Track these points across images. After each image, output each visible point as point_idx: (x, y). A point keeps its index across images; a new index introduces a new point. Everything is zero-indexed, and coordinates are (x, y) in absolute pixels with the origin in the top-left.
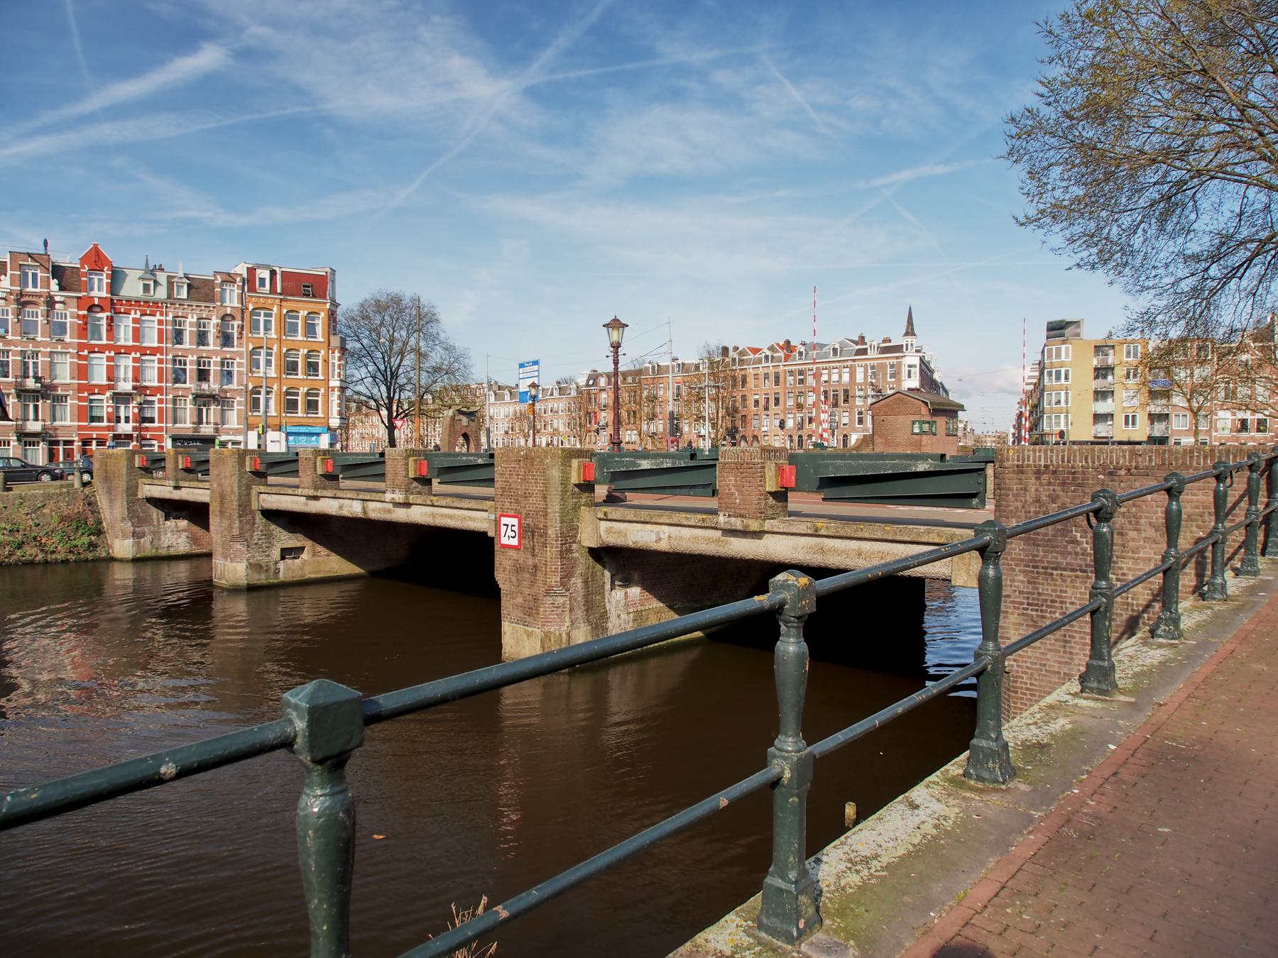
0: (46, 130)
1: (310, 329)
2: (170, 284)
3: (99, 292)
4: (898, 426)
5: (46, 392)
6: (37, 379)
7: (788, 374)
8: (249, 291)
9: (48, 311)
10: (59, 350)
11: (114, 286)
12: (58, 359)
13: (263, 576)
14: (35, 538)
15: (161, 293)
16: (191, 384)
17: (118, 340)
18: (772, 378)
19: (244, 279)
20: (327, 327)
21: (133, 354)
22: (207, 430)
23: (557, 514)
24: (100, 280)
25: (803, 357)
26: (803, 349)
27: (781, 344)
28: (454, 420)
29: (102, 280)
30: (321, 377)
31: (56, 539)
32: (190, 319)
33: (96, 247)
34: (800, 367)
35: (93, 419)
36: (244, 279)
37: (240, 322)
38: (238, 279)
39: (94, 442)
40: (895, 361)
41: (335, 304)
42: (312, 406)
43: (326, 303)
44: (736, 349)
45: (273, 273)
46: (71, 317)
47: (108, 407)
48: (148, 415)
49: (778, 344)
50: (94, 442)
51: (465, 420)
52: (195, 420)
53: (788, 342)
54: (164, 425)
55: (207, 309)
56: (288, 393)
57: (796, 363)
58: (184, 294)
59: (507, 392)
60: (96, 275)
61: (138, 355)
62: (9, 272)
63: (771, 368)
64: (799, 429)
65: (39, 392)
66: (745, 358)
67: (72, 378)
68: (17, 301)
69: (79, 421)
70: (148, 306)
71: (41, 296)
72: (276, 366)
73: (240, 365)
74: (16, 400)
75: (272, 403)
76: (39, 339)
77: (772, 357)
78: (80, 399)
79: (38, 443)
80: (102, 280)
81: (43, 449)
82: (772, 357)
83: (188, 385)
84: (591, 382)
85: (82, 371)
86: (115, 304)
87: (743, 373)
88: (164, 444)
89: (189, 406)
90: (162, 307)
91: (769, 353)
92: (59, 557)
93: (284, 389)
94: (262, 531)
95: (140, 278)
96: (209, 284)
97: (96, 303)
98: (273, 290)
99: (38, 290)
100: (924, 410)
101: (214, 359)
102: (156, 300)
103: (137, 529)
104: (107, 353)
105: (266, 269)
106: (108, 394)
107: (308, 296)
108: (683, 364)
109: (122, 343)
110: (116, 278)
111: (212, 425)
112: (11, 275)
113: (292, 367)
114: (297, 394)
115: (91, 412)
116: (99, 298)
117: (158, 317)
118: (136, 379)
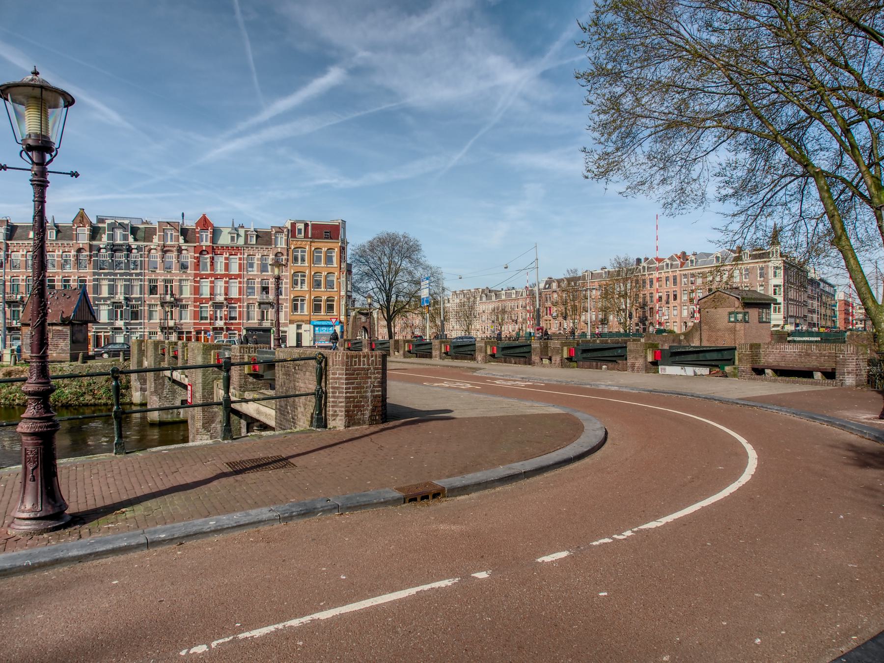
0: (240, 135)
1: (329, 260)
2: (246, 236)
3: (206, 243)
4: (718, 316)
5: (177, 303)
6: (172, 295)
7: (683, 277)
8: (291, 237)
9: (178, 255)
10: (184, 278)
11: (214, 239)
12: (184, 283)
13: (169, 416)
14: (91, 390)
15: (241, 241)
16: (257, 296)
17: (217, 271)
18: (671, 280)
19: (288, 230)
20: (339, 258)
21: (225, 279)
22: (266, 324)
23: (201, 385)
24: (207, 235)
25: (694, 264)
26: (693, 258)
27: (679, 255)
28: (356, 318)
29: (207, 235)
30: (335, 290)
31: (102, 391)
32: (257, 256)
33: (204, 216)
34: (692, 271)
35: (202, 318)
36: (288, 230)
37: (286, 257)
38: (285, 230)
39: (203, 332)
40: (763, 265)
41: (343, 241)
42: (330, 308)
43: (338, 242)
44: (646, 259)
45: (306, 225)
46: (191, 258)
47: (210, 311)
48: (233, 315)
49: (676, 255)
50: (203, 332)
51: (363, 319)
52: (260, 318)
53: (684, 253)
54: (241, 321)
55: (267, 250)
56: (315, 301)
57: (689, 269)
58: (254, 242)
59: (493, 294)
60: (205, 232)
61: (227, 279)
62: (158, 234)
63: (670, 273)
64: (691, 317)
65: (172, 303)
66: (651, 266)
67: (191, 294)
68: (162, 250)
69: (194, 320)
70: (234, 250)
71: (174, 247)
72: (308, 283)
73: (286, 283)
74: (161, 308)
75: (306, 306)
76: (173, 272)
77: (672, 265)
78: (195, 307)
79: (172, 333)
80: (207, 235)
81: (175, 336)
82: (672, 265)
83: (256, 297)
84: (547, 286)
85: (197, 290)
86: (215, 249)
87: (651, 277)
88: (241, 333)
89: (256, 309)
90: (241, 250)
91: (668, 262)
92: (103, 401)
93: (313, 297)
94: (169, 389)
95: (229, 233)
96: (268, 234)
97: (204, 249)
98: (306, 236)
99: (173, 243)
100: (737, 303)
101: (257, 280)
102: (238, 246)
103: (143, 386)
104: (210, 279)
105: (302, 223)
106: (210, 303)
107: (327, 238)
108: (609, 272)
109: (219, 272)
110: (216, 233)
111: (270, 321)
112: (159, 235)
113: (318, 285)
114: (321, 301)
115: (201, 314)
116: (206, 246)
117: (239, 256)
118: (226, 294)
